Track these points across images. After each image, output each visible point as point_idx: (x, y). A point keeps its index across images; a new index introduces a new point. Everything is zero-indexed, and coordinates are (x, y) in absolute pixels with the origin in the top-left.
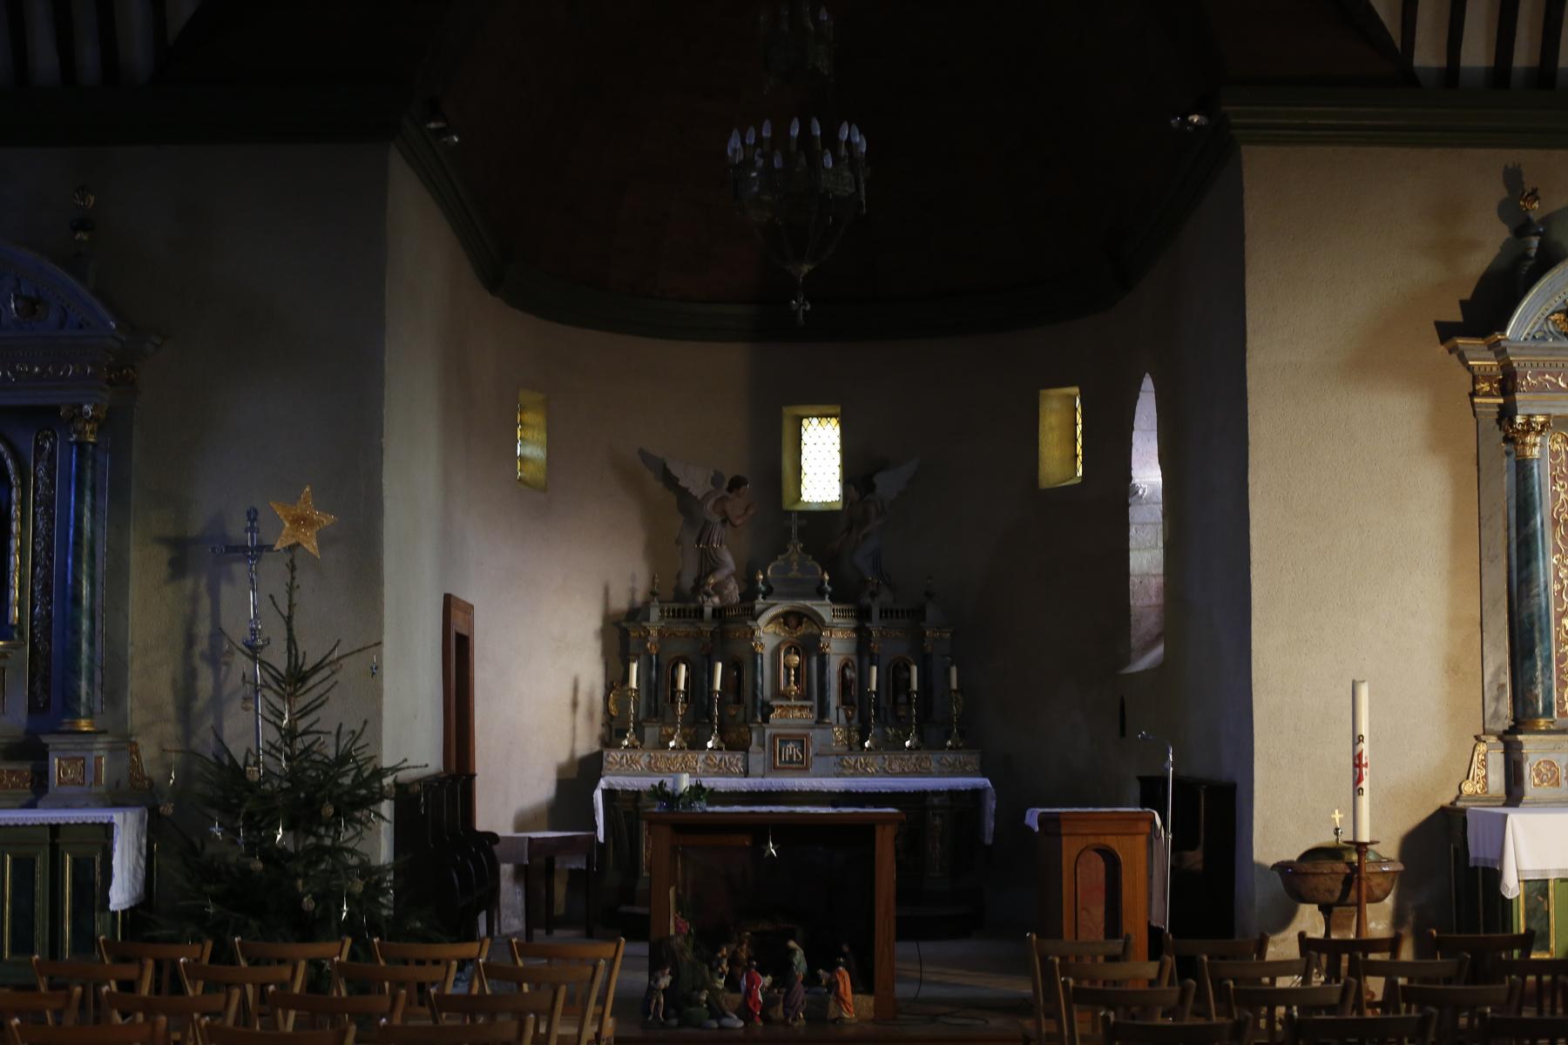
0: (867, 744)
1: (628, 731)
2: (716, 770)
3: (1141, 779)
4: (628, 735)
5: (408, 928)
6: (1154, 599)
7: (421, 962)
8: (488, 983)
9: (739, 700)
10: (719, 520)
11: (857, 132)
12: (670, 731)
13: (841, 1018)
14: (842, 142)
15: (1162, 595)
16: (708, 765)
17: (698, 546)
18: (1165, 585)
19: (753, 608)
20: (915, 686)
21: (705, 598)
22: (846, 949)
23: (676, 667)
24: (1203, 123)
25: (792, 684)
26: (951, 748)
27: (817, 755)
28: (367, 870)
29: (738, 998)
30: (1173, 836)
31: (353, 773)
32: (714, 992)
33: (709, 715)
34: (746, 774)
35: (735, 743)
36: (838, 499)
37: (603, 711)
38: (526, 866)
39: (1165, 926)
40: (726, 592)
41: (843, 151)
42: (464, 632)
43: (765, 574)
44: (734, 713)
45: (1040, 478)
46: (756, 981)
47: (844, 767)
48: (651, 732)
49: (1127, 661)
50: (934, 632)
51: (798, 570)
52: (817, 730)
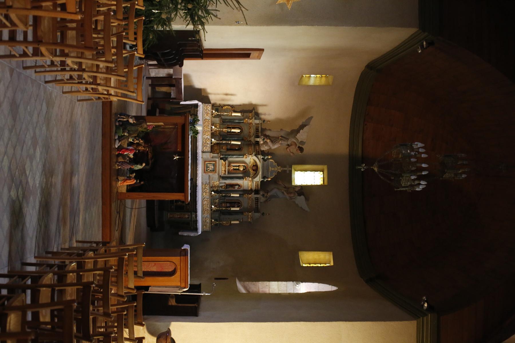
0: (213, 193)
1: (218, 112)
2: (204, 142)
3: (200, 285)
4: (216, 112)
5: (150, 34)
6: (261, 290)
7: (135, 34)
8: (128, 55)
9: (228, 150)
10: (289, 143)
11: (423, 187)
12: (218, 127)
13: (118, 181)
14: (420, 182)
15: (263, 292)
16: (206, 139)
17: (280, 136)
18: (266, 293)
19: (259, 154)
20: (232, 209)
21: (262, 139)
22: (142, 183)
23: (239, 128)
24: (424, 308)
25: (233, 168)
26: (211, 221)
27: (209, 176)
28: (169, 20)
29: (125, 146)
30: (180, 295)
31: (203, 15)
32: (128, 138)
33: (223, 140)
34: (203, 152)
35: (213, 149)
36: (296, 184)
37: (224, 104)
38: (172, 77)
39: (150, 292)
40: (264, 146)
41: (417, 182)
42: (251, 56)
43: (270, 159)
44: (224, 148)
45: (303, 252)
46: (132, 152)
47: (205, 185)
48: (217, 120)
49: (240, 281)
50: (250, 216)
51: (272, 170)
52: (218, 176)
